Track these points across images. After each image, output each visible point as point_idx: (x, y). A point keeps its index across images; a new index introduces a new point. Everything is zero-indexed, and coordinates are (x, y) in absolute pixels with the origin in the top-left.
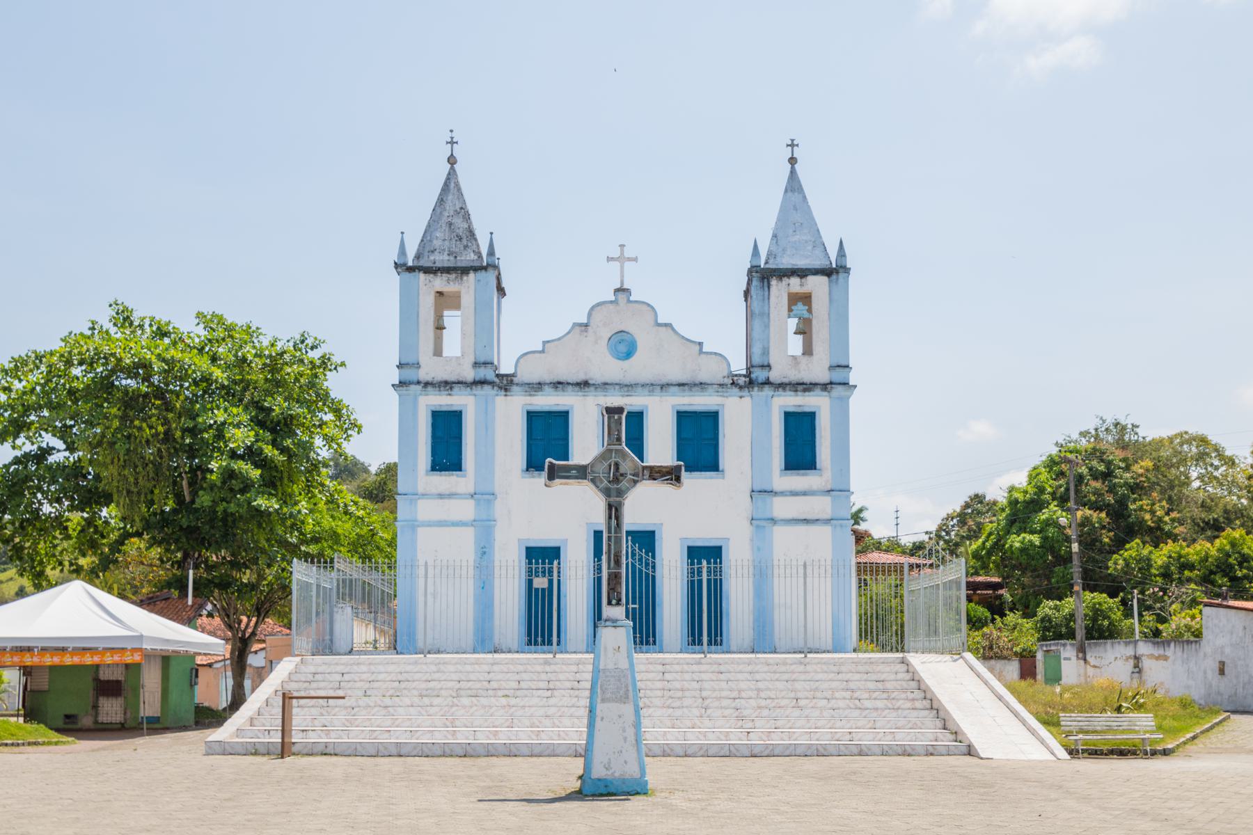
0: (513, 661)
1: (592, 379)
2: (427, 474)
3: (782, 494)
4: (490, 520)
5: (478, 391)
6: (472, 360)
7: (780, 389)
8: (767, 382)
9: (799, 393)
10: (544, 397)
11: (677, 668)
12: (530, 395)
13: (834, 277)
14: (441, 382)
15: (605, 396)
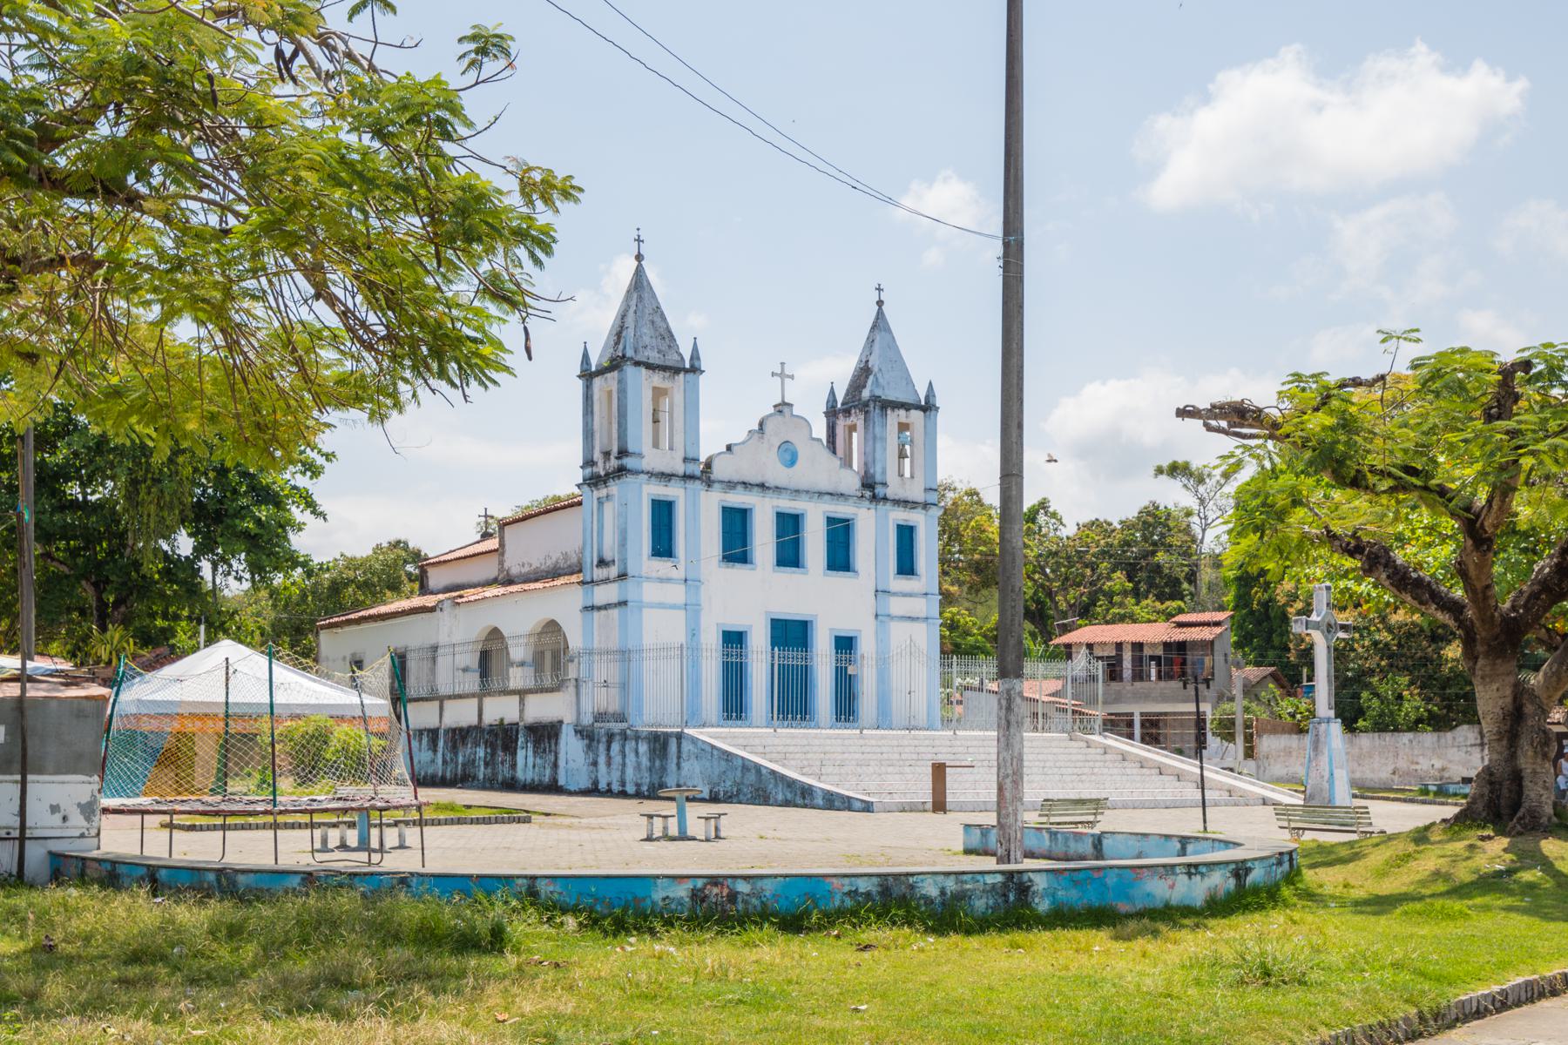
3: (895, 594)
5: (691, 485)
6: (682, 455)
8: (885, 499)
11: (873, 742)
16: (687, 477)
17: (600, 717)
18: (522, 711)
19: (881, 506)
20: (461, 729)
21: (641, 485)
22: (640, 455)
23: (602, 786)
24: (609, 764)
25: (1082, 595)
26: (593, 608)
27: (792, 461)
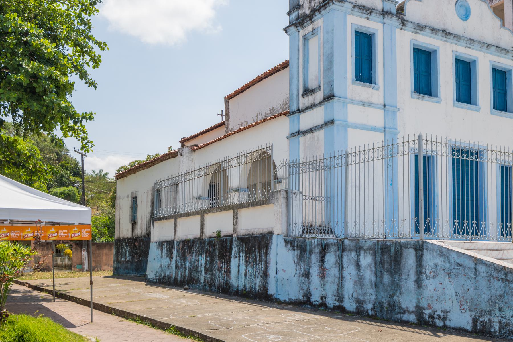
4: (395, 129)
5: (388, 20)
12: (416, 33)
15: (457, 44)
16: (384, 13)
17: (307, 229)
18: (235, 224)
20: (188, 241)
21: (346, 16)
23: (315, 298)
24: (323, 276)
26: (299, 133)
27: (466, 16)
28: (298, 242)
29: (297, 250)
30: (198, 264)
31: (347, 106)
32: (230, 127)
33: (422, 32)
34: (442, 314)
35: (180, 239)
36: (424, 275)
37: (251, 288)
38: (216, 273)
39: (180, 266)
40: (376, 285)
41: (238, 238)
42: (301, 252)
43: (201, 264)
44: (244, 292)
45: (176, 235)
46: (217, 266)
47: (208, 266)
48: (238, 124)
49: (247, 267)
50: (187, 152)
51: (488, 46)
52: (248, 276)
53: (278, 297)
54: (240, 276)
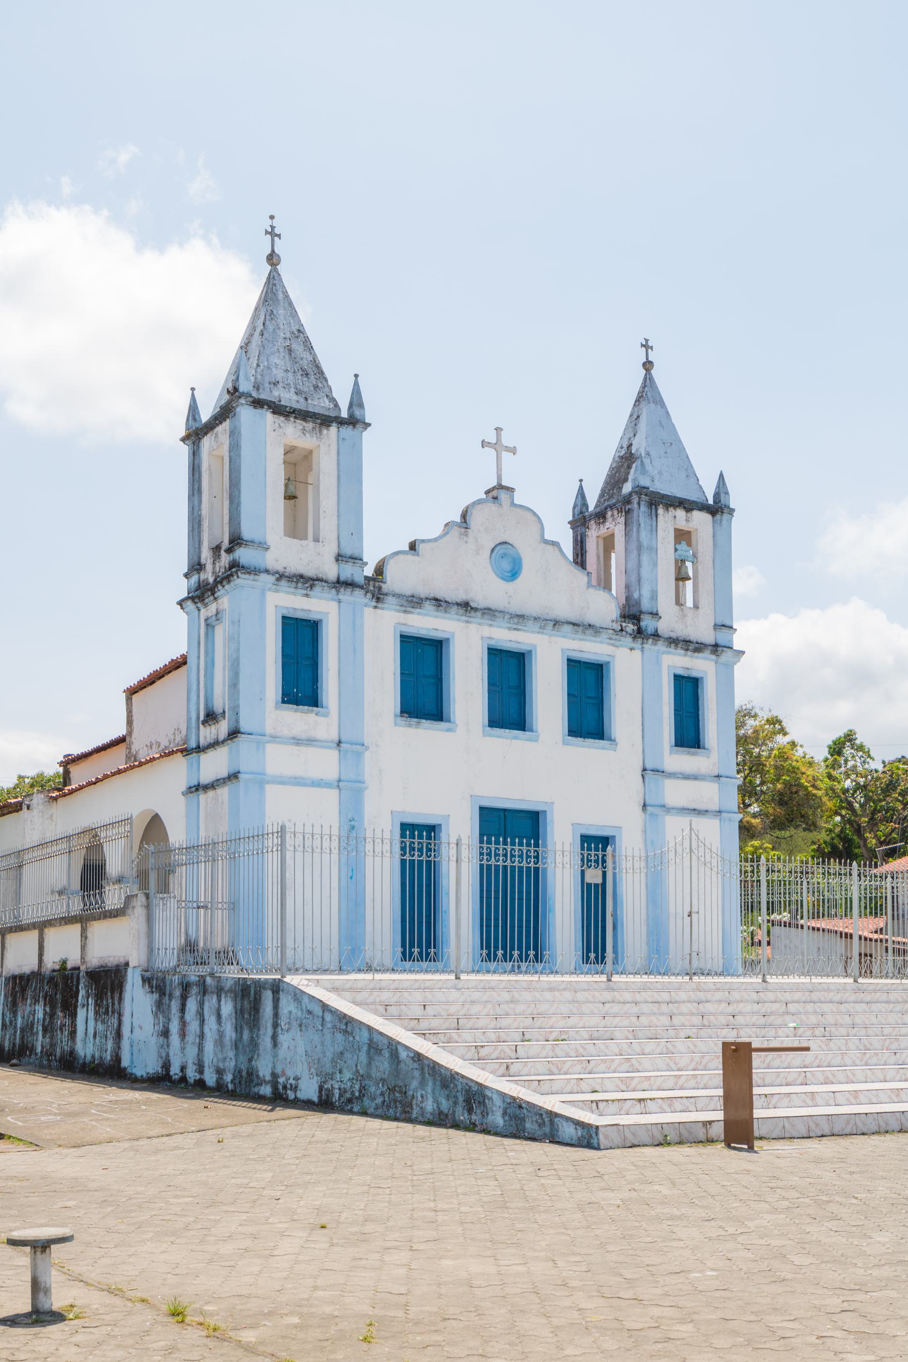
0: (569, 987)
1: (474, 601)
2: (276, 708)
3: (672, 775)
4: (360, 782)
5: (346, 595)
7: (673, 646)
8: (656, 635)
9: (689, 653)
10: (420, 617)
11: (628, 996)
12: (405, 612)
13: (718, 517)
14: (295, 576)
15: (491, 625)
16: (341, 584)
19: (649, 645)
20: (21, 977)
21: (263, 594)
22: (264, 547)
23: (175, 1070)
24: (183, 1034)
25: (893, 831)
27: (513, 573)
28: (157, 979)
29: (156, 992)
30: (34, 1019)
31: (264, 748)
32: (134, 748)
33: (418, 610)
34: (293, 1082)
35: (11, 973)
36: (280, 1028)
37: (101, 1058)
38: (57, 1035)
39: (8, 1023)
40: (236, 1045)
41: (87, 973)
42: (160, 996)
43: (38, 1019)
44: (92, 1066)
45: (4, 965)
46: (59, 1023)
47: (46, 1023)
48: (147, 746)
49: (96, 1022)
50: (41, 802)
51: (555, 625)
52: (98, 1038)
53: (135, 1071)
54: (87, 1039)
